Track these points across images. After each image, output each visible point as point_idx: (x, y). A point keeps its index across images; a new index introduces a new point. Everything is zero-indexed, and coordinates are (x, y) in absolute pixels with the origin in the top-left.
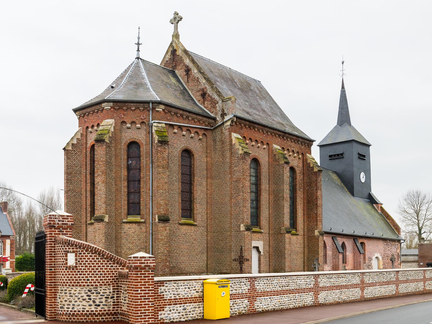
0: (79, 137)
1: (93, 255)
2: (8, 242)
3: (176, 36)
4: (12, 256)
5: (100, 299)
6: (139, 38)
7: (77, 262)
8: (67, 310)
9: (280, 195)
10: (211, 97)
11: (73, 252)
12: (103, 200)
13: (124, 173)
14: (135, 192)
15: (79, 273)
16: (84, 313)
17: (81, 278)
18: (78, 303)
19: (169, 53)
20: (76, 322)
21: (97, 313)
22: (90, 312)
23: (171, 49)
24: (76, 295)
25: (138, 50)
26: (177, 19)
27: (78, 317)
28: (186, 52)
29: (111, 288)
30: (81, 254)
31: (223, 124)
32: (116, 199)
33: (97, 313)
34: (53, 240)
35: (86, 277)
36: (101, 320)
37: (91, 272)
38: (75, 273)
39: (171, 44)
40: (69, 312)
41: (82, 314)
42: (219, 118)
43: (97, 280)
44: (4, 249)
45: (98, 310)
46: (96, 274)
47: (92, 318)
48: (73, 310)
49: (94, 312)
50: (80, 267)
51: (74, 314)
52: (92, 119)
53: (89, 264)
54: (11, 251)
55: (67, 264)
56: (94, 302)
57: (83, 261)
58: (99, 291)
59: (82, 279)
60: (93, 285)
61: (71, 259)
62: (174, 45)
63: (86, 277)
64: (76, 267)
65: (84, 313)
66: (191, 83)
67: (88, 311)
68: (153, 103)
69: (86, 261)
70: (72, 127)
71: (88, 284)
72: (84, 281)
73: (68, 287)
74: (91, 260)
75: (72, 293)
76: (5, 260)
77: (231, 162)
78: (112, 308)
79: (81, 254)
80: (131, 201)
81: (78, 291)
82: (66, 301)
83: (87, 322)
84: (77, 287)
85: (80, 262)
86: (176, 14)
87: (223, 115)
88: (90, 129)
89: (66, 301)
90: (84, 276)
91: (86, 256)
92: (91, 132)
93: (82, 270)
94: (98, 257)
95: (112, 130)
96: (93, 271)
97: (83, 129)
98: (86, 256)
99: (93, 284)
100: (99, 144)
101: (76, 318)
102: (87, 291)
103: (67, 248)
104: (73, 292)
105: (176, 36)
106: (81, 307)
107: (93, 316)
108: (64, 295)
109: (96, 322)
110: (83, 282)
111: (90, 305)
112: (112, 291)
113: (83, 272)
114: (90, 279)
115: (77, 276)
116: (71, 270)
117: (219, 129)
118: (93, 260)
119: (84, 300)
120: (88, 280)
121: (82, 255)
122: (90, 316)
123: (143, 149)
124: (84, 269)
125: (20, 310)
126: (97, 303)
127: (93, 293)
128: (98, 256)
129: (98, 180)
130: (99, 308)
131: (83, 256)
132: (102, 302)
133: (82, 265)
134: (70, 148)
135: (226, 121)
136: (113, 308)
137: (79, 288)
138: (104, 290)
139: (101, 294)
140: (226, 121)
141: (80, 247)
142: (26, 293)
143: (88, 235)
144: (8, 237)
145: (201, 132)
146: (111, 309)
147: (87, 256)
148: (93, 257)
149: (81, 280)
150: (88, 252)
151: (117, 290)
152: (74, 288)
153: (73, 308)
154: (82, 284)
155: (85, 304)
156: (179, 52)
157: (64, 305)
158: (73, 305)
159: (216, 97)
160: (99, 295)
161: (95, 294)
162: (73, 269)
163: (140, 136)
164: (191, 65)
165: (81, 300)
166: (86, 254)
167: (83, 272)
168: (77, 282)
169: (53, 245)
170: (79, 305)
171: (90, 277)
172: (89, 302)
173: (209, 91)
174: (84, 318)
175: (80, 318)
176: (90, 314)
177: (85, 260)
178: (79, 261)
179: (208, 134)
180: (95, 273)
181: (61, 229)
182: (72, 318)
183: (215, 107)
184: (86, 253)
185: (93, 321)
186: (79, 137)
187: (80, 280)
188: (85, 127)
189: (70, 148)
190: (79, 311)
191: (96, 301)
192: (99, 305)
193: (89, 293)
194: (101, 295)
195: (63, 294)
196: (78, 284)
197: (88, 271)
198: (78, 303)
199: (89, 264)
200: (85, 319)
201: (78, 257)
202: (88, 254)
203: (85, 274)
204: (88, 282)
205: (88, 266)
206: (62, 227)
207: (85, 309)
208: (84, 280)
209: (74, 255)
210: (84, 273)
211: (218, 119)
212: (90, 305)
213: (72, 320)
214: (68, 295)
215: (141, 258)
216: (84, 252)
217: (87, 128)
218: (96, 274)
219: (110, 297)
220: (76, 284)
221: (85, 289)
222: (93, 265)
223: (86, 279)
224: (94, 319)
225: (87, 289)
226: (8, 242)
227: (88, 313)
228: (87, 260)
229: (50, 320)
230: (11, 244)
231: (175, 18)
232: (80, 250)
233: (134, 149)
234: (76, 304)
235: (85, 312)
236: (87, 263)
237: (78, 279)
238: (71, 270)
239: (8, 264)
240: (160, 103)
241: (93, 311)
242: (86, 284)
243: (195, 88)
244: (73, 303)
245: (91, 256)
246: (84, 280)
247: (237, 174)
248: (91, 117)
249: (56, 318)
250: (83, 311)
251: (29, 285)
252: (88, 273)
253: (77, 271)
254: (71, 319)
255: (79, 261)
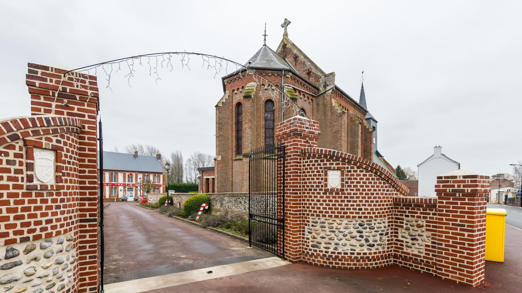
0: (227, 98)
1: (368, 174)
2: (161, 176)
3: (286, 35)
4: (163, 184)
5: (373, 236)
6: (265, 31)
7: (344, 183)
8: (326, 250)
9: (355, 145)
10: (315, 74)
11: (338, 169)
12: (249, 142)
13: (263, 122)
14: (270, 137)
15: (346, 200)
16: (353, 256)
17: (349, 207)
18: (344, 241)
19: (281, 47)
20: (340, 268)
21: (371, 256)
22: (362, 255)
23: (282, 44)
24: (340, 230)
25: (265, 40)
26: (286, 23)
27: (343, 262)
28: (293, 45)
29: (386, 221)
30: (350, 171)
31: (325, 92)
32: (257, 142)
33: (371, 256)
34: (299, 154)
35: (357, 205)
36: (374, 265)
37: (364, 198)
38: (340, 200)
39: (283, 40)
40: (330, 254)
41: (350, 257)
42: (321, 89)
43: (372, 209)
44: (160, 180)
45: (372, 252)
46: (371, 202)
47: (363, 263)
48: (336, 252)
49: (368, 255)
50: (349, 191)
51: (337, 257)
52: (238, 84)
53: (361, 186)
54: (163, 181)
55: (326, 185)
56: (367, 240)
57: (353, 183)
58: (373, 225)
59: (352, 208)
60: (366, 217)
61: (334, 179)
62: (285, 41)
63: (357, 205)
64: (342, 190)
65: (353, 256)
66: (298, 66)
67: (358, 254)
68: (285, 71)
69: (357, 183)
70: (218, 94)
71: (360, 215)
72: (355, 211)
73: (327, 218)
74: (364, 180)
75: (335, 227)
76: (160, 186)
77: (331, 119)
78: (386, 248)
79: (350, 171)
80: (267, 143)
81: (344, 225)
82: (323, 238)
83: (357, 268)
84: (342, 219)
85: (349, 184)
86: (286, 19)
87: (325, 86)
88: (236, 92)
89: (323, 238)
90: (355, 204)
91: (358, 175)
92: (236, 94)
93: (352, 195)
94: (373, 177)
95: (255, 90)
96: (367, 196)
97: (230, 92)
98: (358, 175)
99: (366, 215)
100: (247, 99)
101: (340, 262)
102: (357, 226)
103: (328, 163)
104: (335, 225)
105: (286, 35)
106: (348, 247)
107: (365, 261)
108: (320, 229)
109: (368, 268)
110: (352, 213)
111: (361, 246)
112: (387, 224)
113: (353, 197)
114: (363, 208)
115: (343, 204)
116: (334, 195)
117: (322, 96)
118: (367, 181)
119: (353, 237)
120: (361, 209)
121: (352, 173)
122: (361, 260)
123: (276, 106)
124: (354, 194)
125: (204, 227)
126: (371, 242)
127: (366, 228)
128: (373, 175)
129: (246, 127)
130: (373, 250)
131: (353, 175)
132: (376, 241)
133: (352, 188)
134: (221, 105)
135: (328, 90)
136: (388, 248)
137: (345, 221)
138: (378, 223)
139: (376, 229)
140: (328, 90)
141: (349, 163)
142: (201, 211)
143: (234, 167)
144: (162, 173)
145: (310, 98)
146: (386, 250)
147: (359, 175)
148: (368, 177)
149: (350, 209)
150: (361, 169)
151: (396, 224)
152: (338, 220)
153: (336, 249)
154: (351, 215)
155: (354, 244)
156: (289, 46)
157: (321, 244)
158: (336, 244)
159: (319, 74)
160: (373, 231)
161: (368, 230)
162: (337, 193)
163: (274, 95)
164: (298, 54)
165: (348, 237)
166: (358, 173)
167: (353, 197)
168: (342, 211)
169: (299, 161)
170: (345, 245)
171: (363, 205)
172: (361, 240)
173: (314, 70)
174: (352, 263)
175: (346, 263)
176: (361, 258)
177: (355, 181)
178: (347, 183)
179: (314, 99)
180: (370, 200)
181: (307, 139)
182: (334, 262)
183: (318, 81)
184: (358, 170)
185: (366, 267)
186: (227, 98)
187: (347, 209)
188: (231, 90)
189: (221, 105)
190: (346, 254)
191: (369, 239)
192: (373, 245)
193: (361, 229)
194: (375, 231)
195: (318, 228)
196: (345, 215)
197: (361, 196)
198: (344, 241)
199: (361, 186)
200: (354, 264)
201: (324, 177)
202: (361, 171)
203: (356, 201)
204: (361, 212)
205: (361, 189)
206: (308, 137)
207: (354, 250)
208: (355, 209)
209: (339, 173)
210: (355, 199)
211: (321, 89)
212: (361, 246)
213: (334, 265)
214: (327, 229)
215: (464, 177)
216: (356, 169)
217: (233, 90)
218: (371, 202)
219: (384, 233)
220: (342, 215)
221: (354, 222)
222: (367, 189)
223: (358, 208)
224: (366, 264)
225: (358, 223)
226: (161, 176)
227: (359, 256)
228: (358, 180)
229: (296, 262)
230: (163, 177)
231: (285, 23)
232: (349, 167)
233: (269, 105)
234: (341, 243)
235: (356, 255)
236: (359, 185)
237: (346, 207)
238: (334, 195)
239: (161, 188)
240: (289, 71)
241: (365, 254)
242: (357, 215)
243: (302, 69)
244: (336, 241)
245: (364, 175)
246: (355, 209)
247: (336, 127)
248: (236, 83)
249: (302, 259)
250: (351, 254)
251: (204, 205)
252: (360, 199)
253: (343, 196)
254: (332, 263)
255: (347, 183)
